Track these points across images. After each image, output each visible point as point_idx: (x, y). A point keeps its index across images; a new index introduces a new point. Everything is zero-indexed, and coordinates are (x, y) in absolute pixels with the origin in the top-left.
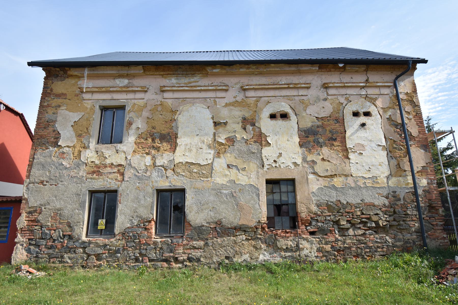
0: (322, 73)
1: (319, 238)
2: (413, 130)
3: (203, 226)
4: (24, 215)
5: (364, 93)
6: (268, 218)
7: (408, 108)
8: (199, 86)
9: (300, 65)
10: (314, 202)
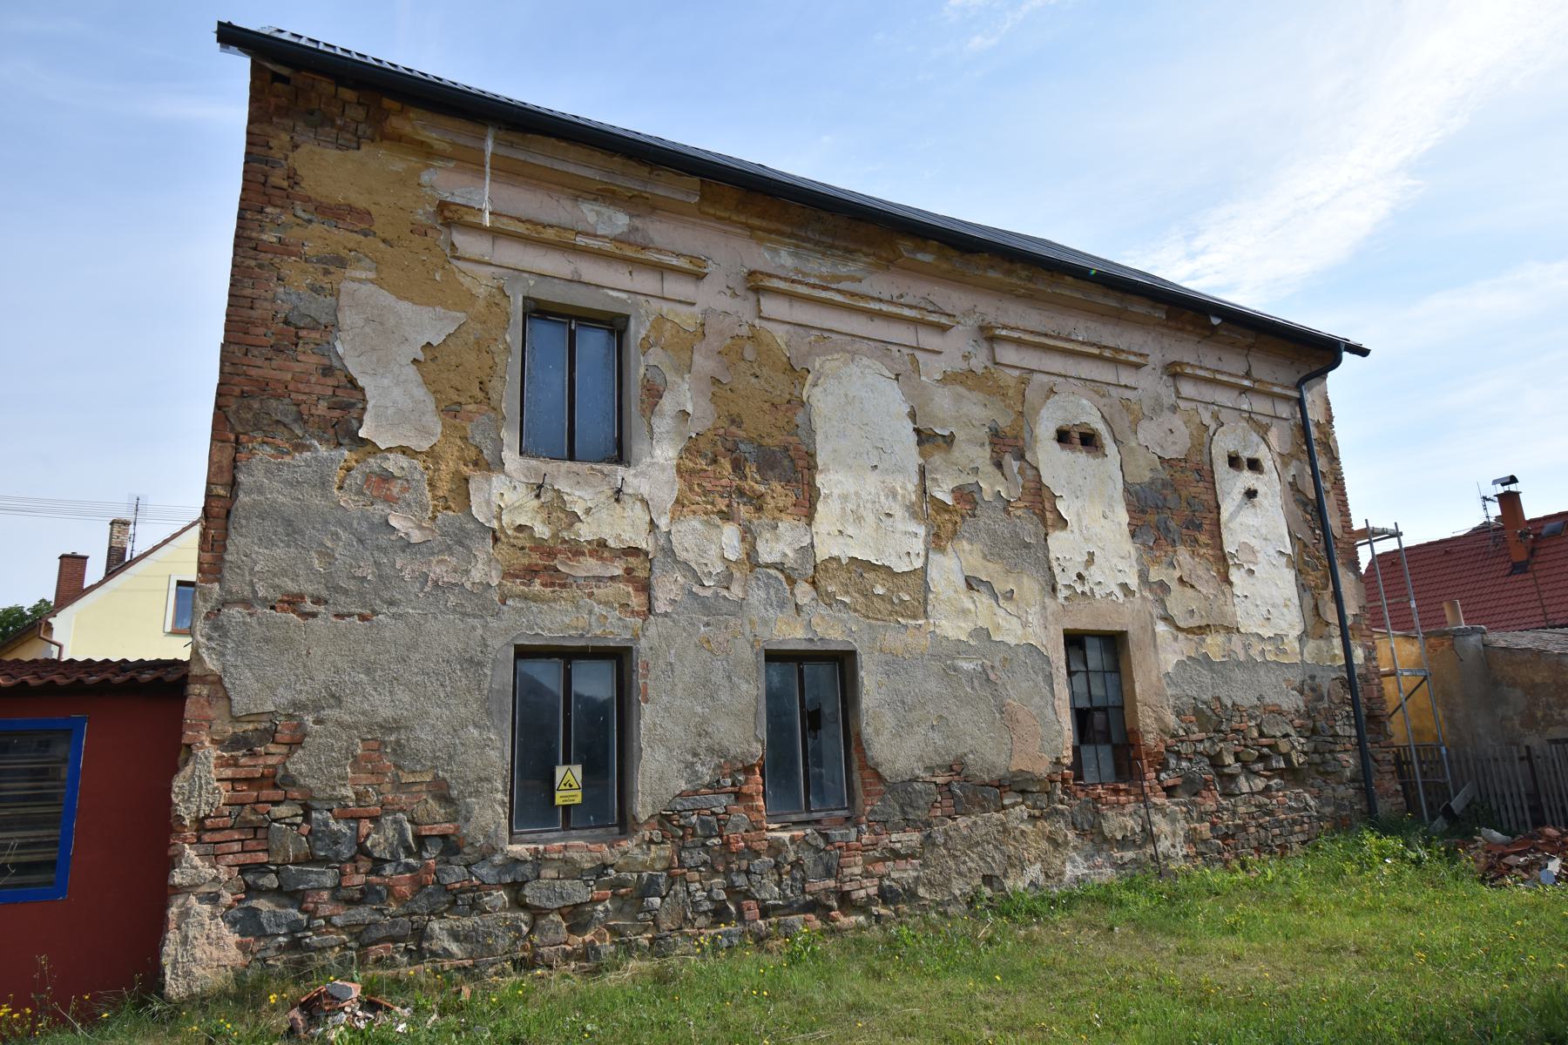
3: (915, 779)
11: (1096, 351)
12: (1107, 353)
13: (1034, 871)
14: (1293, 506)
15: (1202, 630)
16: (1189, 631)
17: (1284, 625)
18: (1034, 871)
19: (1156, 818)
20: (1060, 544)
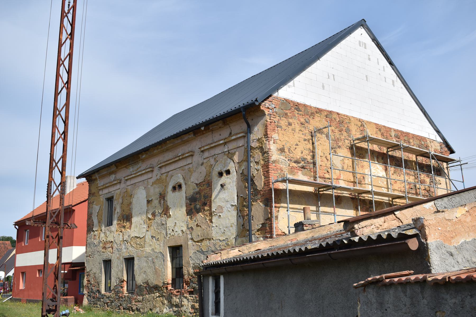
0: (200, 137)
1: (193, 297)
2: (260, 184)
3: (141, 285)
4: (86, 277)
5: (226, 150)
6: (172, 279)
7: (257, 155)
8: (139, 172)
9: (182, 136)
10: (191, 265)
11: (178, 159)
12: (181, 158)
13: (158, 310)
14: (241, 183)
15: (201, 241)
16: (198, 242)
17: (229, 234)
18: (158, 310)
19: (185, 300)
20: (170, 223)
